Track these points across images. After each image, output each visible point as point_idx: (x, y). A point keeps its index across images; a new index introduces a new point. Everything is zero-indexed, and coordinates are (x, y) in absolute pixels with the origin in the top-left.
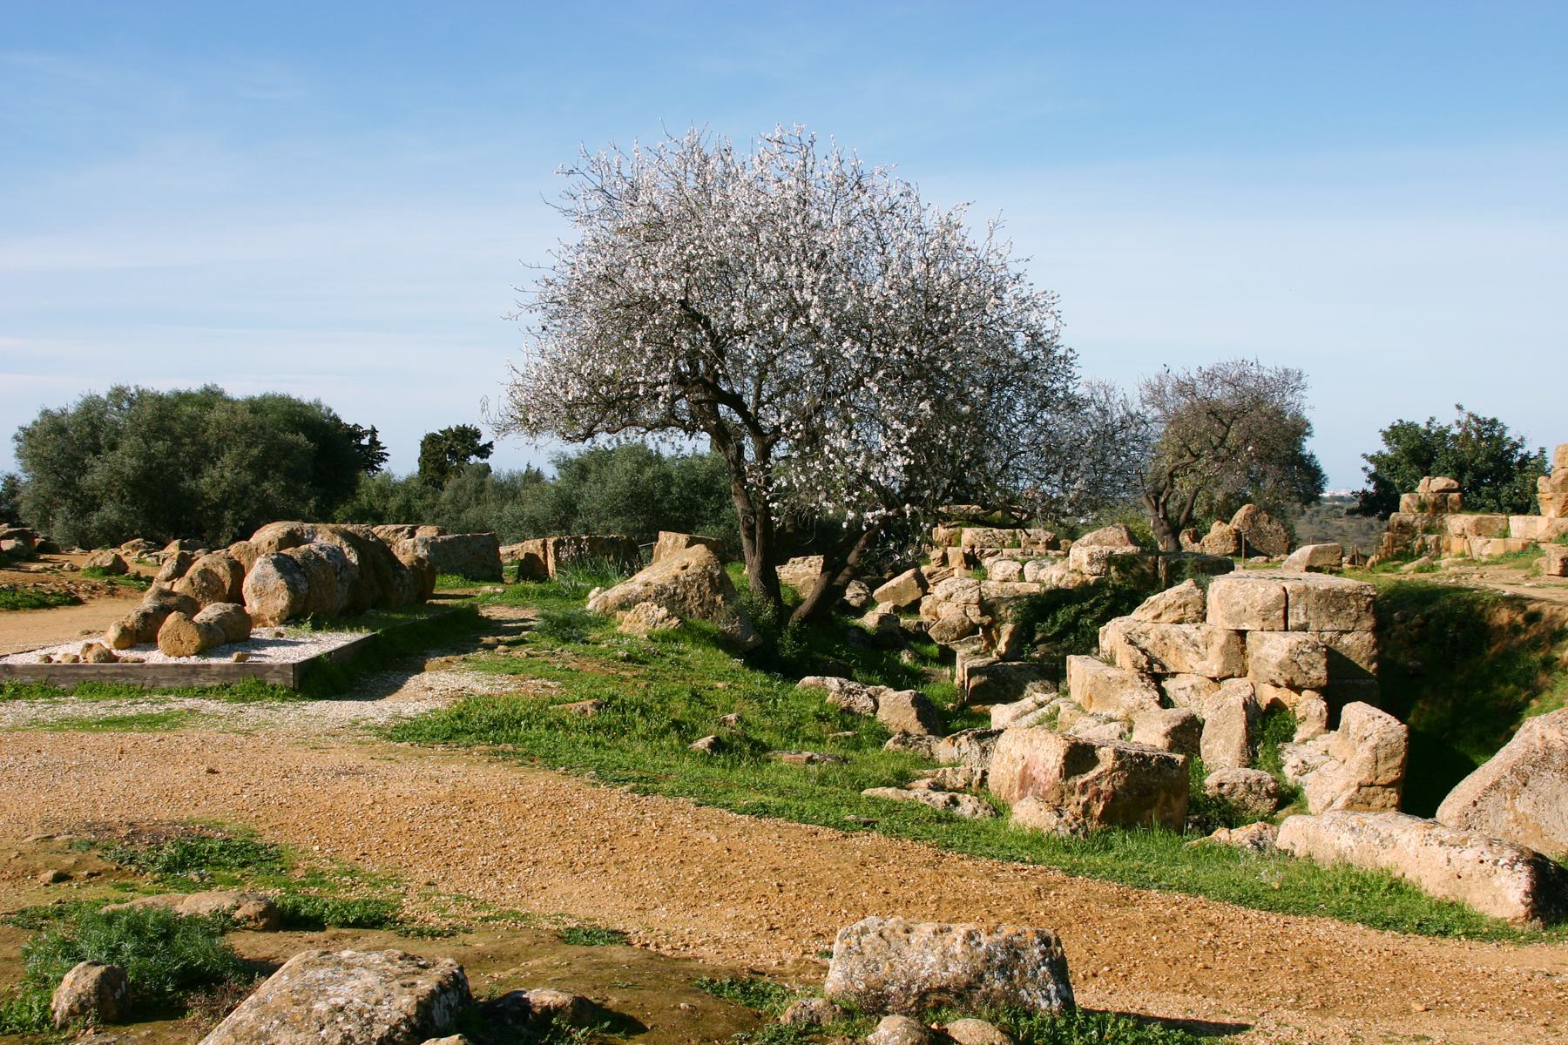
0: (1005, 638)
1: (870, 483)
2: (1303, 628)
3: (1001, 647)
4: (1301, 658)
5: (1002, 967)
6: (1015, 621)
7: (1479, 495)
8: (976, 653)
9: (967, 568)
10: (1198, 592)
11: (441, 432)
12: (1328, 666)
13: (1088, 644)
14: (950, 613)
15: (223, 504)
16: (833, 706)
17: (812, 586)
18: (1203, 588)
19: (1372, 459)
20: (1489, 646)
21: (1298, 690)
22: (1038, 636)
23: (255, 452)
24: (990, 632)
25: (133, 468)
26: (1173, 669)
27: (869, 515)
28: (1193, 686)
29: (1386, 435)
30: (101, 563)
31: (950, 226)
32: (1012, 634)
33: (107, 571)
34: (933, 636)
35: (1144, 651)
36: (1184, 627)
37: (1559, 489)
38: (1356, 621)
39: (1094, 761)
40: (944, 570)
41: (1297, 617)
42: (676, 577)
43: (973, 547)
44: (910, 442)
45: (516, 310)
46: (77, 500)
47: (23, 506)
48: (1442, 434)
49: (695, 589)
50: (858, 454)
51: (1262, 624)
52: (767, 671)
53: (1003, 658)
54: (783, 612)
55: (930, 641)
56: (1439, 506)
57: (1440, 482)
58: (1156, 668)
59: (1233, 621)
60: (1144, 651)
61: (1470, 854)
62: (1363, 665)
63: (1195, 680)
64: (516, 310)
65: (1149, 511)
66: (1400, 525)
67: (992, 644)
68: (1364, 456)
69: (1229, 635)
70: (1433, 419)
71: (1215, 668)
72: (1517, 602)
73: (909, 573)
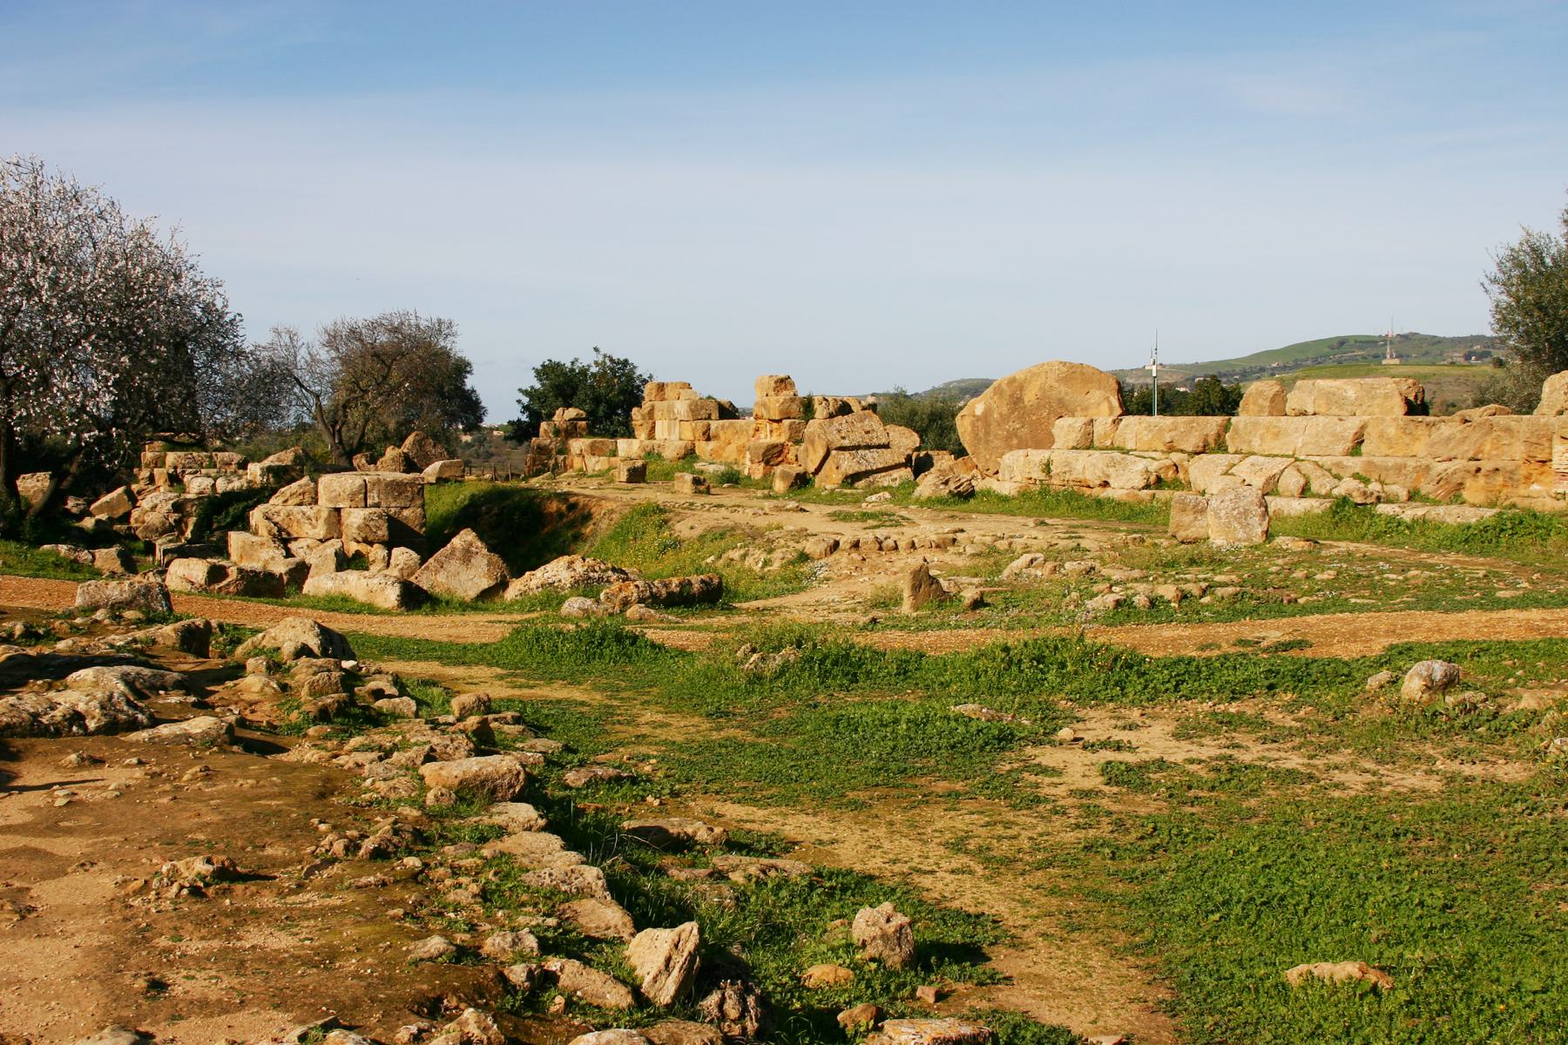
0: (191, 528)
1: (87, 413)
2: (377, 505)
3: (188, 534)
4: (372, 523)
5: (144, 595)
6: (199, 516)
7: (612, 423)
8: (170, 541)
9: (171, 486)
10: (312, 485)
12: (389, 528)
13: (242, 523)
14: (154, 519)
16: (65, 558)
17: (41, 495)
18: (316, 483)
19: (525, 393)
20: (544, 526)
21: (371, 544)
22: (215, 526)
24: (179, 526)
27: (86, 435)
29: (537, 372)
32: (196, 525)
34: (140, 536)
35: (276, 524)
36: (303, 508)
39: (226, 575)
40: (151, 487)
43: (175, 468)
44: (116, 383)
48: (584, 372)
50: (78, 392)
53: (189, 542)
54: (22, 514)
55: (136, 538)
56: (571, 431)
57: (572, 413)
58: (284, 535)
60: (276, 524)
61: (376, 581)
62: (417, 529)
63: (309, 542)
65: (327, 438)
66: (539, 447)
67: (182, 533)
68: (520, 390)
70: (576, 360)
72: (564, 497)
73: (120, 490)
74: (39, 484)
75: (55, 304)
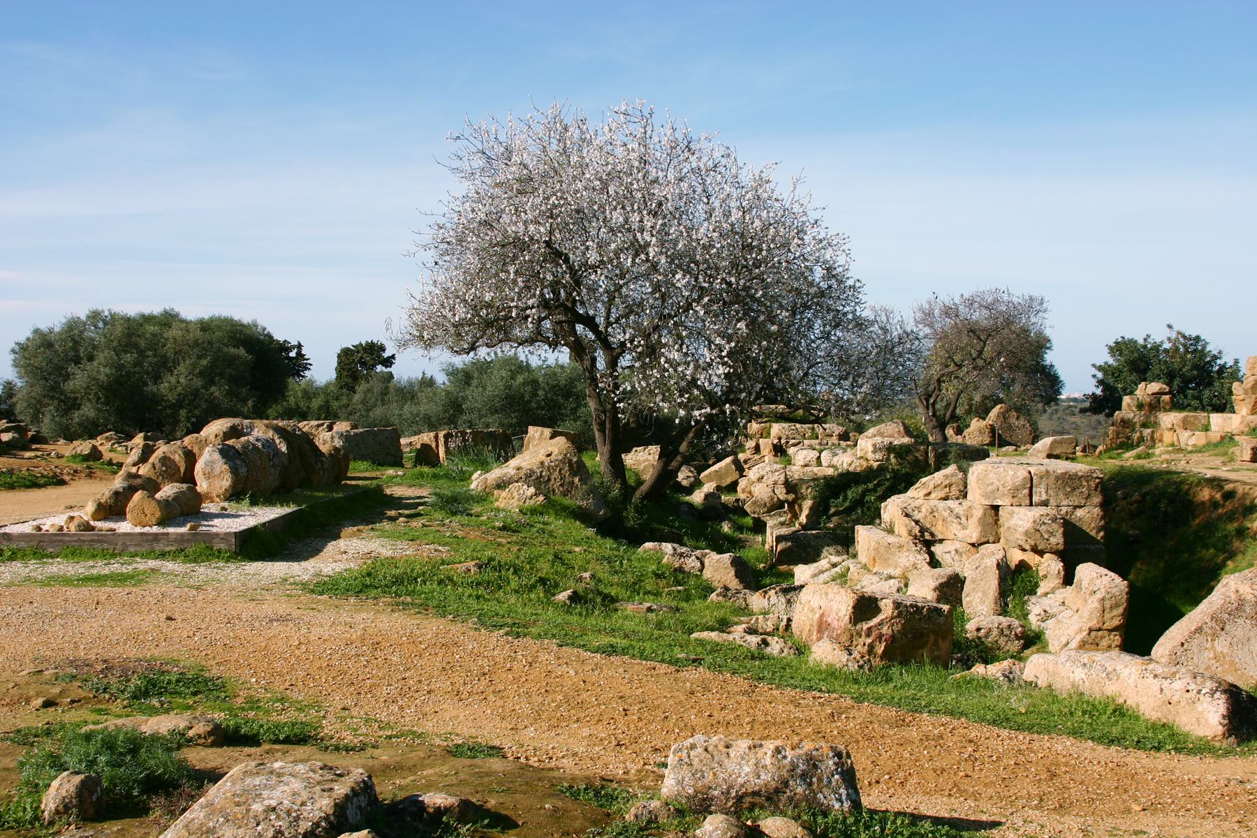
0: (805, 512)
1: (698, 387)
2: (1045, 504)
3: (803, 519)
4: (1043, 528)
5: (804, 776)
6: (814, 498)
7: (1186, 397)
8: (782, 524)
9: (776, 455)
10: (960, 475)
11: (353, 346)
12: (1065, 534)
14: (761, 492)
15: (179, 405)
16: (668, 566)
17: (651, 470)
18: (965, 471)
19: (1100, 368)
20: (1194, 518)
21: (1041, 553)
22: (832, 510)
23: (204, 362)
24: (794, 507)
25: (107, 376)
26: (940, 537)
27: (696, 413)
28: (956, 550)
29: (1111, 349)
30: (81, 451)
31: (762, 182)
32: (811, 509)
33: (86, 458)
34: (748, 510)
35: (917, 522)
36: (949, 503)
37: (1250, 392)
38: (1087, 498)
39: (877, 610)
40: (756, 457)
41: (1040, 495)
42: (542, 463)
43: (780, 439)
44: (730, 355)
45: (413, 249)
46: (62, 401)
47: (18, 406)
48: (1156, 348)
49: (557, 473)
50: (688, 364)
51: (1012, 500)
52: (615, 538)
53: (804, 527)
54: (628, 491)
55: (745, 514)
56: (1154, 406)
57: (1155, 387)
58: (927, 536)
59: (988, 498)
60: (917, 522)
61: (1178, 685)
62: (1093, 533)
63: (958, 545)
64: (414, 249)
66: (1123, 421)
67: (795, 516)
68: (1094, 365)
69: (985, 510)
70: (1148, 336)
71: (974, 536)
72: (1216, 483)
73: (729, 460)
74: (650, 457)
75: (663, 261)
